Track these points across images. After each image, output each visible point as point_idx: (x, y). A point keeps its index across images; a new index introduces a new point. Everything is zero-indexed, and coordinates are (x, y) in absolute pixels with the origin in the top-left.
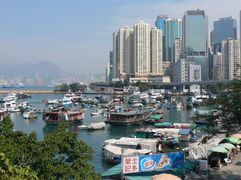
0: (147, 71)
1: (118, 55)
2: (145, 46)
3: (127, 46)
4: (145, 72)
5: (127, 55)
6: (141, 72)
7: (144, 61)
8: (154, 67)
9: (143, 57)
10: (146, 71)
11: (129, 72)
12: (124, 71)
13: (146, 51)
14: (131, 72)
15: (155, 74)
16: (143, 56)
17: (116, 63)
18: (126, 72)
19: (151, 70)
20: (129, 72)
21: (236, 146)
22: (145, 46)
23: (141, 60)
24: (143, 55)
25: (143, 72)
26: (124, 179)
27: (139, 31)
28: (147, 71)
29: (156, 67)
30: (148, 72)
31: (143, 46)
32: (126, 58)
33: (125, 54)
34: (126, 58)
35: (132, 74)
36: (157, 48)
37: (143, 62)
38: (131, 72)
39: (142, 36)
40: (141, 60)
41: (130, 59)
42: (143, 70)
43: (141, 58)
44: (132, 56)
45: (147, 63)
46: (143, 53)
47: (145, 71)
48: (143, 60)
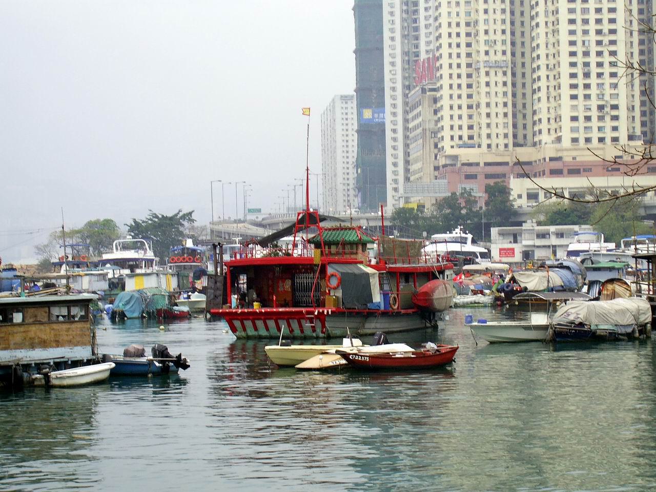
1: (417, 38)
2: (605, 22)
5: (486, 32)
6: (582, 136)
7: (600, 65)
9: (593, 37)
11: (502, 141)
12: (471, 137)
14: (516, 145)
18: (485, 142)
21: (250, 289)
23: (580, 59)
24: (592, 27)
25: (595, 135)
26: (642, 2)
27: (573, 130)
28: (623, 135)
31: (592, 22)
34: (483, 48)
38: (516, 145)
42: (595, 123)
46: (592, 16)
48: (593, 59)
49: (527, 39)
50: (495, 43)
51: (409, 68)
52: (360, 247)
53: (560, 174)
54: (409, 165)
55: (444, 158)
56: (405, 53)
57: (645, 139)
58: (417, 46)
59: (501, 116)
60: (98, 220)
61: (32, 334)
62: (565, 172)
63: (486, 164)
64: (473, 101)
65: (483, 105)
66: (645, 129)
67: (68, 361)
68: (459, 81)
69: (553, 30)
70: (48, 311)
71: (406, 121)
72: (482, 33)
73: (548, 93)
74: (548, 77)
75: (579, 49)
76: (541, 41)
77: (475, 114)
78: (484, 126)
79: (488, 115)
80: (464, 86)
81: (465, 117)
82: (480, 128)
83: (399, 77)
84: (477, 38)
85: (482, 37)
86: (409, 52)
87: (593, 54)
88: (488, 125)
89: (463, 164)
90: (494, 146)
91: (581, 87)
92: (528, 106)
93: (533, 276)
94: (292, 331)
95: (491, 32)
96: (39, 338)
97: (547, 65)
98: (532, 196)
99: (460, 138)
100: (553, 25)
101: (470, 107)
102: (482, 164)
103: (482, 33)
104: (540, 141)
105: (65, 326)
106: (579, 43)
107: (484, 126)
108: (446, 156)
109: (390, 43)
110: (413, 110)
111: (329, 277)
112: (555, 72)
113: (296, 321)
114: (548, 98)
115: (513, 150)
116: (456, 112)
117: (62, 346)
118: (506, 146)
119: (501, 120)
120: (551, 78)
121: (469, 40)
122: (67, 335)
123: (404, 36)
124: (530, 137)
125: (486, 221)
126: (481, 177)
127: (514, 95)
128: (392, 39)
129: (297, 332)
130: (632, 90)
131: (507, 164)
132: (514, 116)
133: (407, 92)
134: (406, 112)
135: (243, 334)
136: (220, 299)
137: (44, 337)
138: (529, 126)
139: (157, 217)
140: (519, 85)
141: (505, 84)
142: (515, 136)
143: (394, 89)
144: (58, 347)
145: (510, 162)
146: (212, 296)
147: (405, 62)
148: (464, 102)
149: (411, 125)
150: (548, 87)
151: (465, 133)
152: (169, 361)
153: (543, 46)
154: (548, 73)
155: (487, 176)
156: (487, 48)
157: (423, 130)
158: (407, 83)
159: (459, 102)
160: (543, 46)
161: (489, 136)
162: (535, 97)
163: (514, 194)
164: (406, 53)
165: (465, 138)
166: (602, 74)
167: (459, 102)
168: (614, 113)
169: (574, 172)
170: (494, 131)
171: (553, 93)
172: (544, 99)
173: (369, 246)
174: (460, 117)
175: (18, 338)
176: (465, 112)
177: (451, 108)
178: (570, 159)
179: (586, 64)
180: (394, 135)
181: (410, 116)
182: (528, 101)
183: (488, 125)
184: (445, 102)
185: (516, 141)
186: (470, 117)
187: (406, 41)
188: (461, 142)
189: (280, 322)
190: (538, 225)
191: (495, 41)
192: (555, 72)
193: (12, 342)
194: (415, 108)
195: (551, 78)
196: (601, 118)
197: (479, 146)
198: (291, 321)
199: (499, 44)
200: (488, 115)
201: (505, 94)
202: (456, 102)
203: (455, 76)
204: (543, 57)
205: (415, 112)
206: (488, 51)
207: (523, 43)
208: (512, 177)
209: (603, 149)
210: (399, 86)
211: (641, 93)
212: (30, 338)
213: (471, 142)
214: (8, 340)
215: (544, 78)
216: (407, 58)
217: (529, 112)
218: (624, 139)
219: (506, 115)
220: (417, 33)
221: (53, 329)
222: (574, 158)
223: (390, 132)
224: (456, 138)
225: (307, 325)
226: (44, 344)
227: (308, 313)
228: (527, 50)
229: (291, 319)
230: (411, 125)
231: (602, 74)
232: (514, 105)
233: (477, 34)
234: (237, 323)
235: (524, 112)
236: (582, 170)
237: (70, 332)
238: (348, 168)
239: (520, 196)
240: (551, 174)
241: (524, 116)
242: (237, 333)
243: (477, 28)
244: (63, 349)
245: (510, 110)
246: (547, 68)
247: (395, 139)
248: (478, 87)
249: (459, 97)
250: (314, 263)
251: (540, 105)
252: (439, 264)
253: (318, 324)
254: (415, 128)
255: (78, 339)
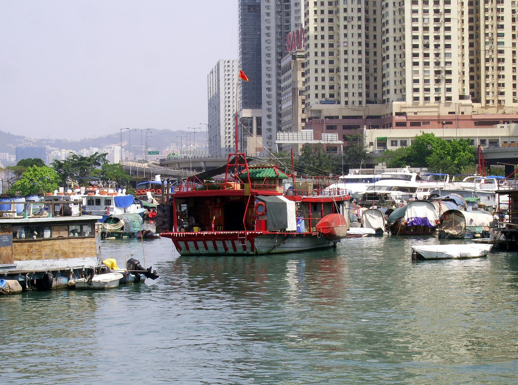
0: (455, 95)
1: (288, 14)
2: (442, 38)
3: (346, 69)
4: (443, 99)
5: (345, 10)
8: (490, 73)
9: (432, 15)
10: (449, 90)
11: (357, 99)
12: (332, 96)
13: (446, 55)
14: (368, 102)
15: (492, 113)
16: (431, 12)
17: (281, 55)
18: (343, 99)
19: (472, 86)
20: (357, 99)
22: (442, 38)
23: (420, 33)
28: (455, 95)
29: (499, 68)
30: (462, 97)
32: (342, 23)
33: (338, 70)
34: (342, 23)
35: (374, 109)
36: (503, 60)
37: (432, 47)
38: (368, 102)
39: (427, 64)
40: (420, 33)
41: (363, 31)
43: (420, 77)
44: (371, 16)
45: (455, 51)
47: (443, 91)
48: (431, 33)
49: (378, 16)
50: (352, 19)
51: (281, 38)
52: (278, 182)
53: (404, 126)
54: (281, 117)
55: (310, 112)
56: (278, 26)
57: (473, 98)
58: (288, 21)
59: (356, 78)
60: (30, 159)
61: (56, 247)
62: (408, 124)
63: (344, 117)
64: (334, 66)
65: (342, 69)
66: (473, 90)
67: (82, 269)
68: (323, 50)
69: (399, 9)
70: (67, 229)
71: (279, 81)
72: (341, 11)
73: (395, 60)
74: (395, 47)
75: (419, 24)
76: (390, 18)
77: (335, 76)
78: (342, 87)
79: (346, 78)
80: (327, 54)
81: (327, 79)
82: (340, 88)
83: (273, 45)
84: (338, 15)
85: (342, 14)
86: (281, 25)
87: (431, 29)
88: (346, 86)
89: (326, 117)
90: (350, 103)
91: (421, 55)
92: (379, 70)
93: (24, 245)
94: (226, 249)
95: (349, 10)
96: (62, 250)
97: (395, 38)
98: (382, 142)
99: (323, 95)
100: (400, 5)
101: (331, 71)
102: (340, 118)
103: (341, 11)
104: (388, 99)
105: (80, 241)
106: (420, 20)
107: (342, 87)
108: (311, 111)
109: (266, 17)
110: (284, 73)
111: (257, 208)
112: (400, 43)
113: (230, 242)
114: (395, 64)
115: (366, 107)
116: (320, 75)
117: (77, 257)
118: (360, 103)
119: (356, 81)
120: (397, 48)
121: (331, 16)
122: (80, 248)
123: (278, 13)
124: (379, 96)
125: (345, 164)
126: (340, 128)
127: (367, 62)
128: (268, 14)
129: (231, 251)
130: (463, 59)
131: (361, 117)
132: (367, 79)
133: (280, 58)
134: (278, 74)
135: (186, 252)
136: (167, 225)
137: (66, 249)
138: (379, 86)
139: (77, 158)
140: (371, 54)
141: (360, 52)
142: (368, 95)
143: (269, 55)
144: (74, 257)
145: (363, 116)
146: (161, 222)
147: (278, 33)
148: (327, 66)
149: (283, 85)
150: (395, 55)
151: (327, 92)
152: (141, 273)
153: (391, 22)
154: (395, 44)
155: (345, 127)
156: (346, 23)
157: (293, 89)
158: (280, 51)
159: (323, 67)
160: (391, 22)
161: (346, 95)
162: (385, 63)
163: (367, 141)
164: (279, 26)
165: (327, 96)
166: (439, 45)
167: (323, 67)
168: (448, 77)
169: (415, 124)
170: (350, 90)
171: (399, 61)
172: (392, 65)
173: (284, 181)
174: (323, 79)
175: (47, 250)
176: (327, 75)
177: (316, 71)
178: (413, 114)
179: (426, 38)
180: (268, 93)
181: (282, 77)
182: (379, 66)
183: (346, 86)
184: (312, 67)
185: (368, 99)
186: (332, 79)
187: (279, 17)
188: (324, 100)
189: (217, 242)
190: (387, 168)
191: (352, 17)
192: (400, 43)
193: (43, 253)
194: (286, 72)
195: (397, 48)
196: (438, 81)
197: (339, 103)
198: (226, 241)
199: (356, 19)
200: (346, 78)
201: (360, 61)
202: (320, 67)
203: (319, 46)
204: (391, 31)
205: (286, 74)
206: (346, 25)
207: (375, 20)
208: (365, 129)
209: (438, 107)
210: (273, 53)
211: (470, 62)
212: (56, 251)
213: (331, 99)
214: (40, 251)
215: (391, 48)
216: (280, 30)
217: (379, 75)
218: (455, 99)
219: (360, 77)
220: (289, 10)
221: (71, 243)
222: (416, 113)
223: (266, 90)
224: (320, 96)
225: (239, 244)
226: (65, 255)
227: (241, 235)
228: (378, 25)
229: (226, 240)
230: (283, 85)
231: (439, 45)
232: (367, 70)
233: (338, 12)
234: (182, 244)
235: (375, 75)
236: (422, 123)
237: (83, 246)
238: (229, 119)
239: (371, 144)
240: (396, 126)
241: (375, 79)
242: (182, 252)
243: (338, 6)
244: (78, 259)
245: (363, 73)
246: (395, 40)
247: (269, 96)
248: (338, 55)
249: (323, 62)
250: (245, 195)
251: (388, 70)
252: (339, 196)
253: (248, 244)
254: (287, 87)
255: (88, 251)
